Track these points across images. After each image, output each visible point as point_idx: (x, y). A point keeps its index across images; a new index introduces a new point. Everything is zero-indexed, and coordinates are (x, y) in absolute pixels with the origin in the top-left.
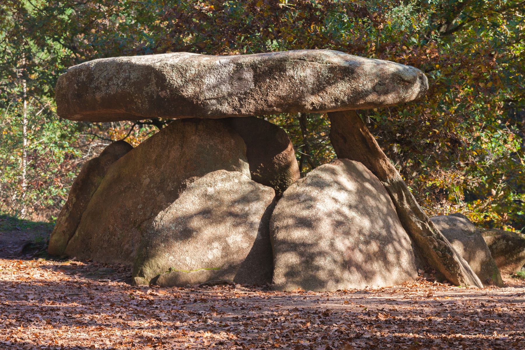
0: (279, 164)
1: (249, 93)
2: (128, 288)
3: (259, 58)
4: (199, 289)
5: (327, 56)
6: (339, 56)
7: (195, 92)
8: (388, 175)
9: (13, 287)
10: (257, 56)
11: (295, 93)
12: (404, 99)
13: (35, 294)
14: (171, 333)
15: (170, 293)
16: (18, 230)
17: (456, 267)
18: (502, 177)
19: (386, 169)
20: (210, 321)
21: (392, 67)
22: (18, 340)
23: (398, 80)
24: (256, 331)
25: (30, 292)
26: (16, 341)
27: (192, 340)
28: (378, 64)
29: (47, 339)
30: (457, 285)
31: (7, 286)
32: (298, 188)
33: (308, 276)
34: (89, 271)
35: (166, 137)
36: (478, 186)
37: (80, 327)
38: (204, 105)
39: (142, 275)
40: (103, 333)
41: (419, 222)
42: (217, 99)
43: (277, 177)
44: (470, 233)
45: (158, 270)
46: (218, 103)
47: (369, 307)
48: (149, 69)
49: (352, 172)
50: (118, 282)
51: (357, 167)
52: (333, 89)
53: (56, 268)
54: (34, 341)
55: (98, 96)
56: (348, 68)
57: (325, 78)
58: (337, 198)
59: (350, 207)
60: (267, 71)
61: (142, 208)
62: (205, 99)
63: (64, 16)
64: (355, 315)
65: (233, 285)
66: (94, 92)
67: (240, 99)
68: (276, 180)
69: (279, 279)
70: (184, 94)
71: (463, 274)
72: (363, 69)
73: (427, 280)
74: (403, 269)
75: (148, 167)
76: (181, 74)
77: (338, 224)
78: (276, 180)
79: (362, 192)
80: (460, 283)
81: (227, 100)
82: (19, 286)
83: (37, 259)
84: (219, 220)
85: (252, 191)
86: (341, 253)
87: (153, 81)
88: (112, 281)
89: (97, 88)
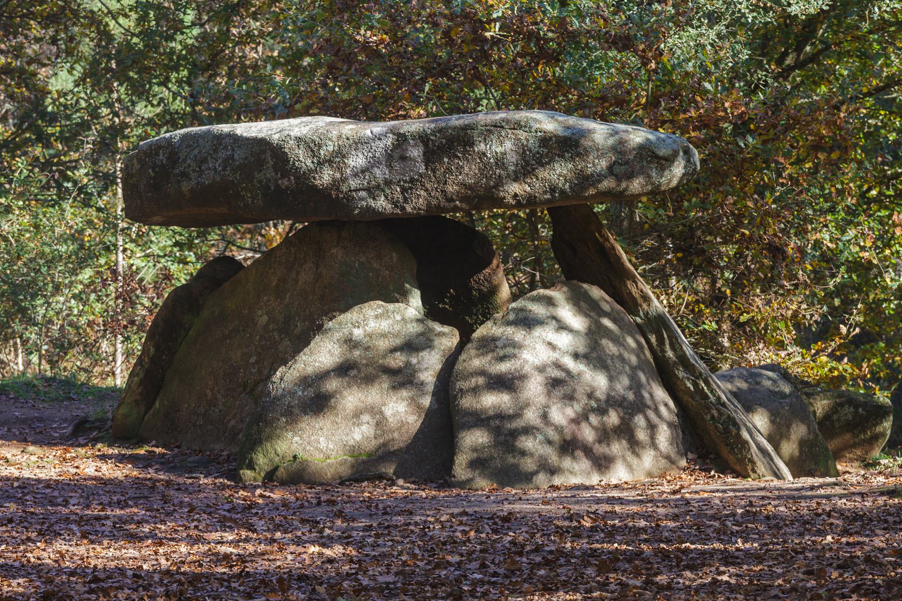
0: (480, 290)
1: (417, 180)
2: (228, 486)
3: (433, 126)
4: (337, 488)
5: (536, 120)
6: (557, 120)
7: (334, 180)
8: (641, 306)
9: (48, 486)
10: (429, 122)
11: (489, 178)
12: (660, 185)
13: (82, 497)
14: (262, 547)
15: (290, 494)
16: (74, 400)
17: (745, 448)
18: (856, 305)
19: (637, 296)
20: (327, 531)
21: (638, 136)
22: (32, 560)
23: (649, 156)
24: (390, 543)
25: (73, 494)
26: (29, 561)
27: (290, 557)
28: (617, 133)
29: (76, 558)
30: (745, 476)
31: (40, 486)
32: (494, 328)
33: (505, 464)
34: (173, 462)
35: (293, 250)
36: (819, 320)
37: (130, 542)
38: (348, 200)
39: (251, 467)
40: (161, 551)
41: (688, 379)
42: (368, 190)
43: (477, 311)
44: (783, 395)
45: (277, 459)
46: (370, 197)
47: (575, 508)
48: (261, 144)
49: (581, 302)
50: (215, 478)
51: (591, 293)
52: (547, 172)
53: (121, 459)
54: (56, 561)
55: (186, 187)
56: (570, 139)
57: (534, 155)
58: (555, 343)
59: (576, 356)
60: (444, 146)
61: (257, 362)
62: (350, 191)
63: (173, 45)
64: (549, 520)
65: (393, 480)
66: (179, 182)
67: (404, 190)
68: (476, 314)
69: (460, 469)
70: (318, 182)
71: (755, 458)
72: (593, 141)
73: (700, 469)
74: (661, 452)
75: (266, 298)
76: (312, 151)
77: (554, 383)
78: (476, 314)
79: (595, 333)
80: (751, 473)
81: (384, 191)
82: (60, 486)
83: (93, 446)
84: (369, 380)
85: (422, 334)
86: (559, 429)
87: (268, 163)
88: (205, 477)
89: (185, 175)
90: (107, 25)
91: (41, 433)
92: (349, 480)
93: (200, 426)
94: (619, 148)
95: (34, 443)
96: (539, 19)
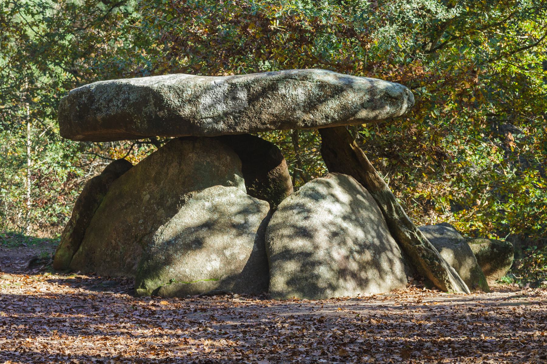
1: (243, 112)
13: (42, 306)
16: (25, 246)
17: (444, 274)
18: (486, 188)
25: (37, 305)
31: (15, 300)
33: (306, 285)
34: (93, 284)
35: (165, 155)
38: (200, 124)
40: (108, 343)
48: (147, 90)
52: (324, 106)
53: (61, 282)
55: (99, 117)
57: (315, 96)
61: (143, 223)
62: (202, 118)
66: (95, 114)
67: (235, 118)
70: (182, 113)
75: (148, 184)
76: (178, 94)
79: (355, 205)
80: (448, 289)
83: (43, 274)
87: (151, 101)
89: (99, 110)
90: (25, 31)
91: (9, 266)
92: (205, 295)
93: (108, 262)
94: (372, 91)
95: (6, 272)
96: (302, 18)
